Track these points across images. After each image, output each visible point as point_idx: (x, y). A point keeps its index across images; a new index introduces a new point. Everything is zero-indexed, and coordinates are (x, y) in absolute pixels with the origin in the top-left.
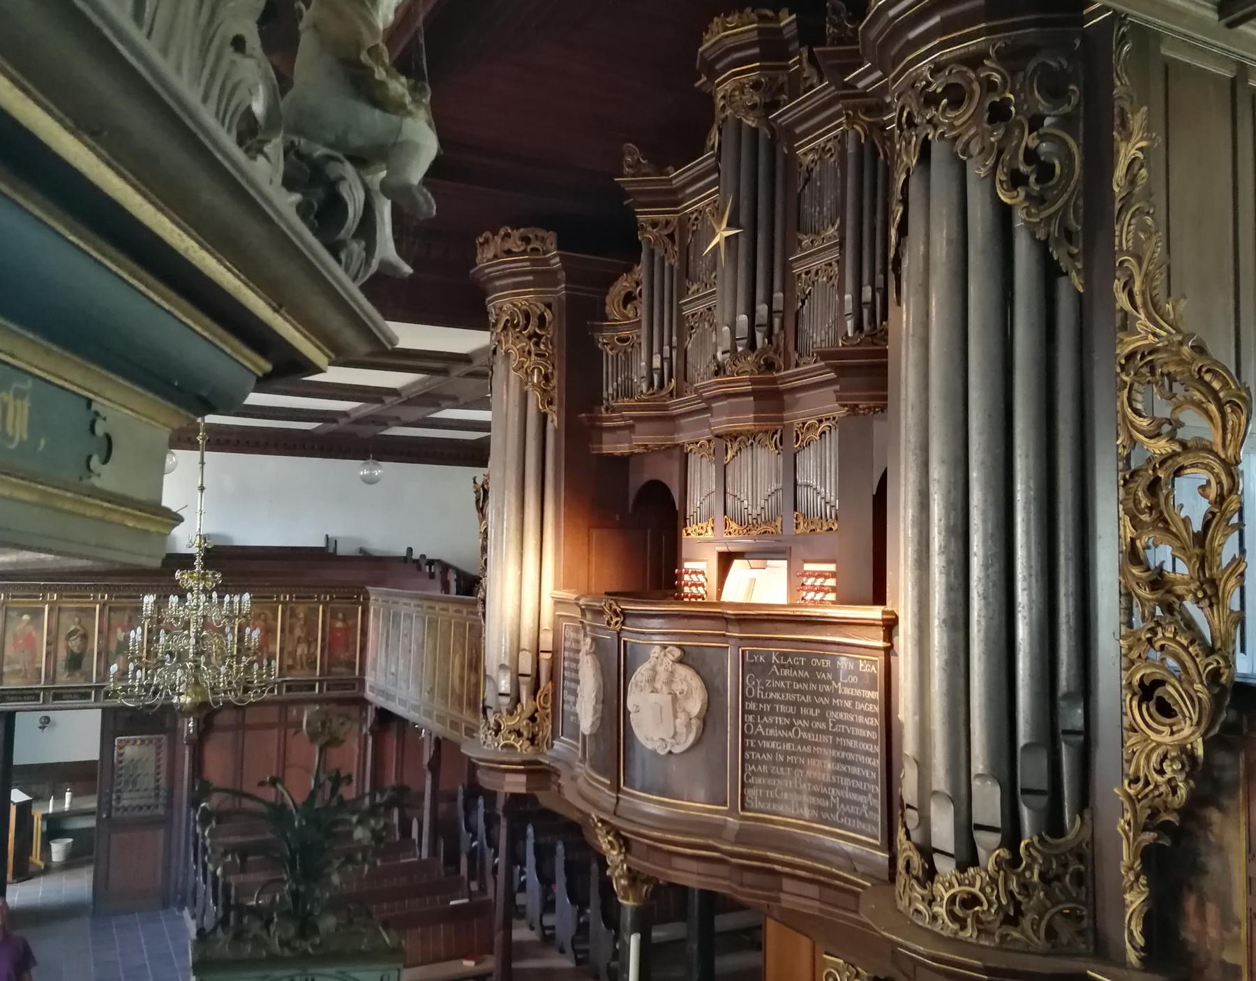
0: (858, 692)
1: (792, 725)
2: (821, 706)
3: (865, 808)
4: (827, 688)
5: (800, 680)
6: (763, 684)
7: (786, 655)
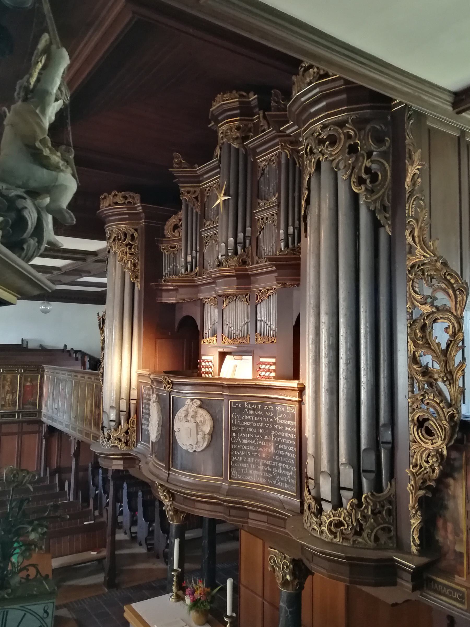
0: (286, 422)
1: (254, 438)
2: (268, 428)
3: (289, 478)
4: (271, 420)
5: (258, 416)
6: (240, 418)
7: (252, 404)
